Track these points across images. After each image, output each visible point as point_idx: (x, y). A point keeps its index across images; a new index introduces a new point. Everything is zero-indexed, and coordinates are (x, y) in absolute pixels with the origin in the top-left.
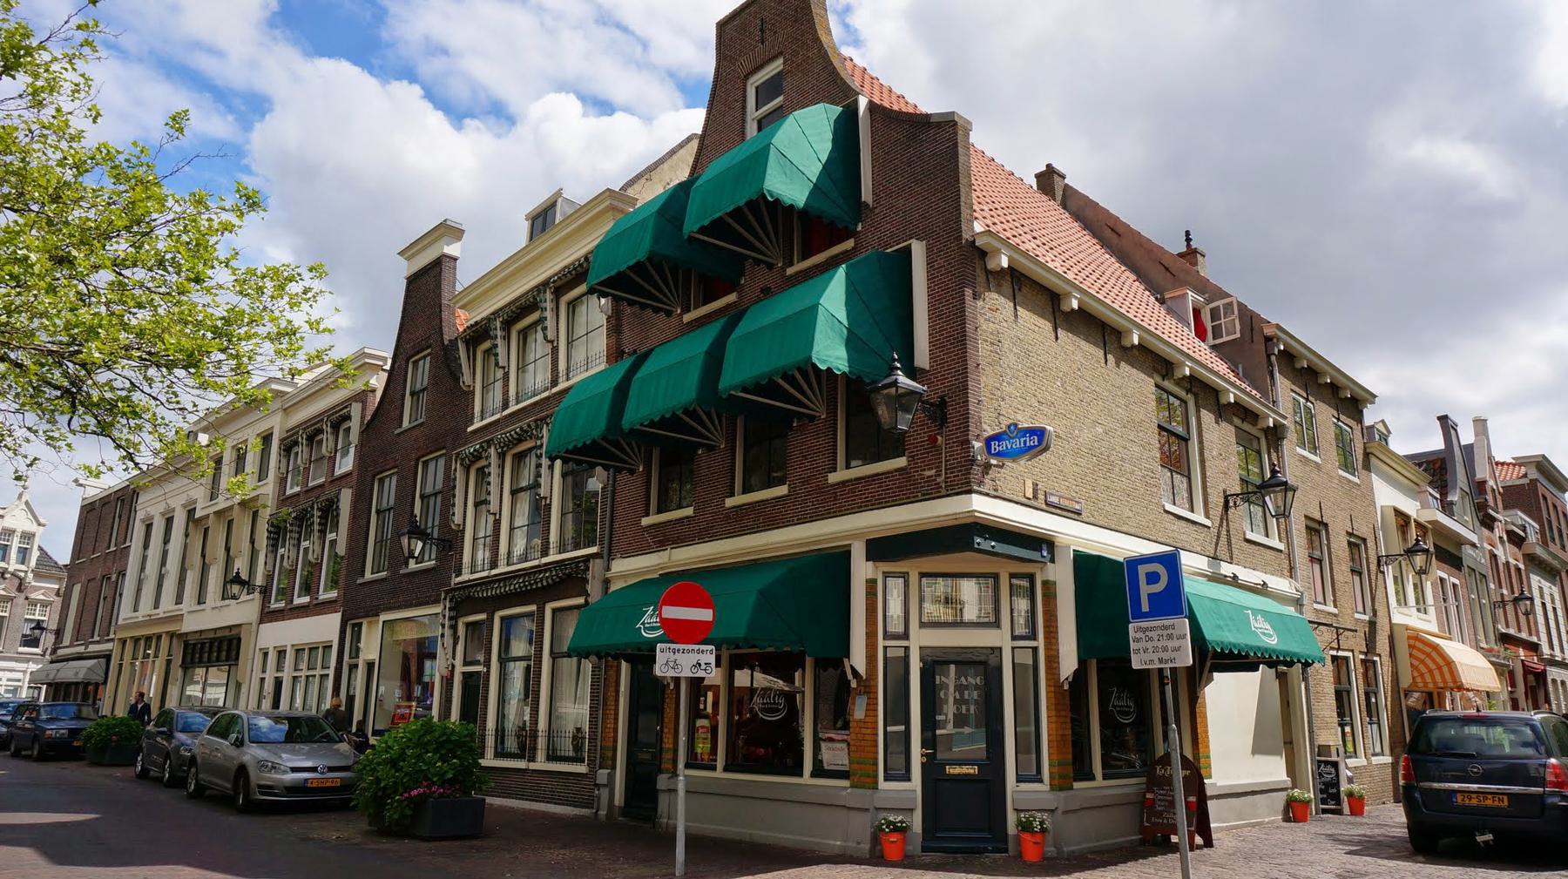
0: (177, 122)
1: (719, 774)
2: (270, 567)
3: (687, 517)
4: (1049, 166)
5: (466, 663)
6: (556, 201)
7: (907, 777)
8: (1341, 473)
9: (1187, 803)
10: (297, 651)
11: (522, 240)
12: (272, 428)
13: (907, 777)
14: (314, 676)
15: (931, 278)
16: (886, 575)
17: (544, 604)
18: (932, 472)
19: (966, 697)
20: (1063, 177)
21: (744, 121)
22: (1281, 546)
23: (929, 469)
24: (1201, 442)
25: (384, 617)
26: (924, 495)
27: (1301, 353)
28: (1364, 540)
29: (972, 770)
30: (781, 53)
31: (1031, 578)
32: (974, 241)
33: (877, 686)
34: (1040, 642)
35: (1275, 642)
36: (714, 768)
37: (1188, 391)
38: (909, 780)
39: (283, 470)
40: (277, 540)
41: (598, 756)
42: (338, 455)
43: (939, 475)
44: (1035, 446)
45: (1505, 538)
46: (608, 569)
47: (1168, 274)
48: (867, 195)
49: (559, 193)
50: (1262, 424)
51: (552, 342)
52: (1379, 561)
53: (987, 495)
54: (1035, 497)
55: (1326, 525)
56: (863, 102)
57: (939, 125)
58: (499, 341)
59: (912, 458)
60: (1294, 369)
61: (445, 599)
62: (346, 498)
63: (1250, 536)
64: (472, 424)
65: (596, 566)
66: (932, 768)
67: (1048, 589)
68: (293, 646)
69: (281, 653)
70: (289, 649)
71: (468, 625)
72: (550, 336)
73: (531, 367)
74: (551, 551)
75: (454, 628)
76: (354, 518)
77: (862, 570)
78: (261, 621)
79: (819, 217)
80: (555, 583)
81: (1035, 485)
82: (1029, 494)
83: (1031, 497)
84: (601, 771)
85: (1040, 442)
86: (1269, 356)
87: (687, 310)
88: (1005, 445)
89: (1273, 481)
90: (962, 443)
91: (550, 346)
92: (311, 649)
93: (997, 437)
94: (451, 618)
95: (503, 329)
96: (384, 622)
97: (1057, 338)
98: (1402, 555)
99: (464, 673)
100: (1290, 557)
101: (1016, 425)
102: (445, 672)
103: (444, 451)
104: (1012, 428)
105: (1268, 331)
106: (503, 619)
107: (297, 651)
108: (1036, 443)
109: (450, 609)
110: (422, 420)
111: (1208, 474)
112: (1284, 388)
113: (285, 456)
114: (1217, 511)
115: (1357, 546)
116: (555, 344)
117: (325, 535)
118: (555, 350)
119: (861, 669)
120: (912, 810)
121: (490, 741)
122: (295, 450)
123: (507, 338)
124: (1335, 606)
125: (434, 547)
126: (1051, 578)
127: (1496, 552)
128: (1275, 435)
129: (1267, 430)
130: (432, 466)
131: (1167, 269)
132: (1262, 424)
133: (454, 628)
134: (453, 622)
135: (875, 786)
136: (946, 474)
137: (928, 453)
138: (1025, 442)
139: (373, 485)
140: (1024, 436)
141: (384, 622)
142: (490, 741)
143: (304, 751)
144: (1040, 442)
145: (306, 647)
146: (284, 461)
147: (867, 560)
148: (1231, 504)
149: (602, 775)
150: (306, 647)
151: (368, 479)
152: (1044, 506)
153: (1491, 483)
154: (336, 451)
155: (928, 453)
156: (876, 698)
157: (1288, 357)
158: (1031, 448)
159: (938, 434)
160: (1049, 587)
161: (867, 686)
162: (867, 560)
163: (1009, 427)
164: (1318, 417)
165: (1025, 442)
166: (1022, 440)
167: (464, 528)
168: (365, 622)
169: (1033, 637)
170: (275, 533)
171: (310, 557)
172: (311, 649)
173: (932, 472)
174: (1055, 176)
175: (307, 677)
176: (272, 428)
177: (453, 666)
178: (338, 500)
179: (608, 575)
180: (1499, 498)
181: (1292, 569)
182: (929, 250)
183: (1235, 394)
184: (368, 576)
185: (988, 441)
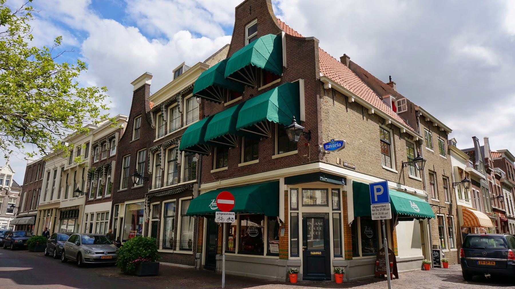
0: (58, 40)
1: (236, 254)
2: (89, 187)
3: (226, 170)
4: (344, 55)
5: (153, 218)
6: (183, 66)
7: (298, 256)
8: (441, 155)
9: (390, 264)
10: (98, 214)
11: (172, 79)
12: (89, 141)
13: (298, 256)
14: (103, 222)
15: (306, 92)
16: (291, 189)
17: (179, 199)
18: (306, 155)
19: (317, 229)
20: (349, 58)
21: (244, 40)
22: (421, 180)
23: (305, 154)
24: (394, 145)
25: (126, 203)
26: (303, 163)
27: (427, 116)
28: (448, 178)
29: (319, 253)
30: (256, 18)
31: (339, 190)
32: (320, 79)
33: (288, 226)
34: (342, 211)
35: (419, 211)
36: (234, 253)
37: (390, 129)
38: (299, 256)
39: (93, 154)
40: (91, 177)
41: (196, 249)
42: (111, 149)
43: (309, 156)
44: (340, 147)
45: (494, 177)
46: (200, 187)
47: (384, 90)
48: (285, 64)
49: (184, 64)
50: (414, 140)
51: (181, 112)
52: (453, 185)
53: (324, 163)
54: (340, 163)
55: (436, 173)
56: (283, 34)
57: (308, 41)
58: (164, 112)
59: (299, 151)
60: (425, 121)
61: (146, 197)
62: (114, 164)
63: (410, 176)
64: (155, 139)
65: (196, 186)
66: (306, 253)
67: (344, 193)
68: (96, 212)
69: (92, 215)
70: (95, 213)
71: (154, 205)
72: (181, 110)
73: (174, 121)
74: (181, 181)
75: (149, 206)
76: (116, 170)
77: (283, 187)
78: (86, 204)
79: (269, 71)
80: (182, 192)
81: (340, 160)
82: (338, 162)
83: (339, 163)
84: (197, 253)
85: (342, 145)
86: (417, 117)
87: (225, 102)
88: (330, 146)
89: (418, 158)
90: (316, 146)
91: (181, 114)
92: (102, 213)
93: (327, 144)
94: (148, 203)
95: (165, 108)
96: (126, 204)
97: (347, 111)
98: (460, 183)
99: (152, 221)
100: (424, 183)
101: (334, 140)
102: (146, 221)
103: (146, 148)
104: (332, 141)
105: (416, 109)
106: (165, 203)
107: (98, 214)
108: (340, 146)
109: (148, 200)
110: (138, 138)
111: (397, 156)
112: (422, 127)
113: (94, 150)
114: (400, 168)
115: (446, 179)
116: (182, 113)
117: (107, 176)
118: (182, 115)
119: (283, 220)
120: (299, 266)
121: (161, 244)
122: (97, 148)
123: (167, 111)
124: (439, 199)
125: (143, 180)
126: (345, 190)
127: (491, 181)
128: (419, 143)
129: (416, 142)
130: (142, 153)
131: (383, 88)
132: (414, 140)
133: (149, 206)
134: (149, 205)
135: (287, 259)
136: (311, 156)
137: (305, 149)
138: (337, 145)
139: (123, 159)
140: (336, 143)
141: (126, 204)
142: (161, 244)
143: (100, 247)
144: (342, 145)
145: (101, 213)
146: (93, 152)
147: (285, 184)
148: (404, 166)
149: (198, 255)
150: (101, 213)
151: (121, 157)
152: (343, 167)
153: (490, 159)
154: (110, 148)
155: (305, 149)
156: (288, 230)
157: (423, 117)
158: (339, 147)
159: (308, 143)
160: (345, 193)
161: (285, 226)
162: (285, 184)
163: (331, 140)
164: (433, 137)
165: (337, 145)
166: (336, 145)
167: (152, 174)
168: (120, 205)
169: (339, 209)
170: (90, 175)
171: (102, 183)
172: (102, 213)
173: (306, 155)
174: (347, 58)
175: (101, 223)
176: (89, 141)
177: (149, 219)
178: (111, 164)
179: (200, 189)
180: (492, 164)
181: (424, 187)
182: (305, 82)
183: (405, 130)
184: (121, 189)
185: (325, 145)
